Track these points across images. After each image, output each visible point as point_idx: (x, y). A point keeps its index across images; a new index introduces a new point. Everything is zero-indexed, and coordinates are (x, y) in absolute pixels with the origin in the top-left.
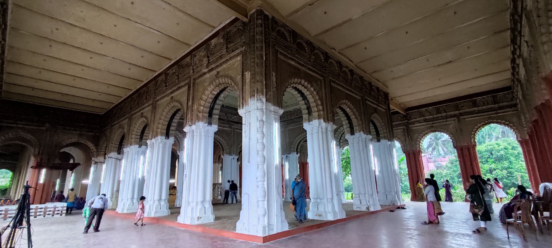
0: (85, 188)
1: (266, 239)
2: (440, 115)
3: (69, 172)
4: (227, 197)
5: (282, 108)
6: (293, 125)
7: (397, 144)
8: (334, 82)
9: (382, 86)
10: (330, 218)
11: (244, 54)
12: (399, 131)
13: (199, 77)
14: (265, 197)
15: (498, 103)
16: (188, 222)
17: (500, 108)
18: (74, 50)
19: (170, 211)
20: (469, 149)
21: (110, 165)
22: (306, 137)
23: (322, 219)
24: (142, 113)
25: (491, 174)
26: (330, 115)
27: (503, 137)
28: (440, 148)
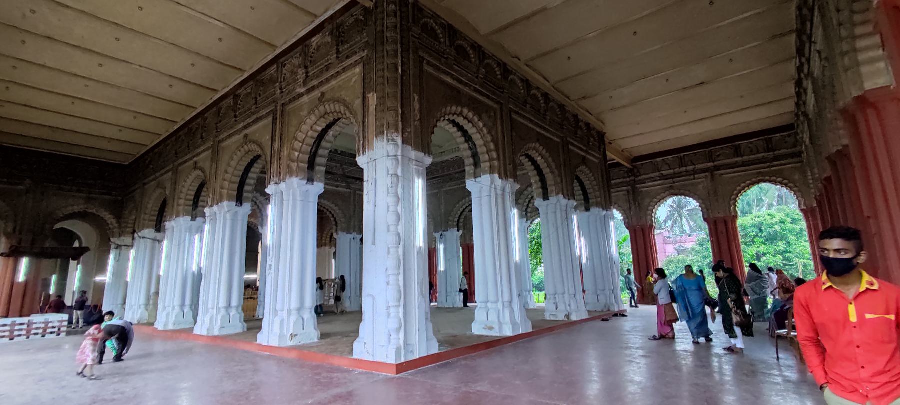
1: (401, 368)
2: (684, 169)
3: (73, 263)
4: (337, 305)
6: (450, 184)
7: (618, 215)
8: (518, 113)
9: (595, 120)
10: (508, 332)
11: (366, 63)
12: (619, 194)
14: (400, 301)
15: (774, 151)
16: (275, 343)
17: (776, 159)
18: (69, 50)
19: (246, 325)
20: (726, 223)
22: (471, 205)
23: (494, 335)
24: (196, 163)
28: (684, 221)
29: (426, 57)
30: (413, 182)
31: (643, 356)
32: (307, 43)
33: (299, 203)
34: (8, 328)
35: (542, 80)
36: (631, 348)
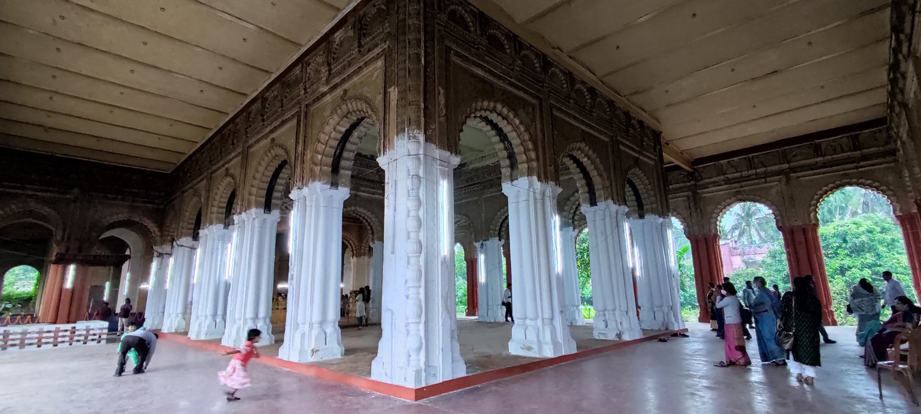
0: (144, 296)
1: (420, 393)
2: (754, 171)
4: (359, 317)
5: (456, 154)
7: (676, 222)
8: (560, 110)
9: (649, 118)
10: (549, 353)
11: (387, 55)
12: (679, 200)
13: (314, 101)
15: (860, 149)
16: (295, 359)
17: (865, 158)
19: (273, 337)
20: (804, 231)
21: (180, 260)
24: (227, 169)
25: (844, 275)
26: (551, 169)
27: (864, 212)
28: (753, 231)
29: (454, 47)
30: (437, 183)
31: (708, 388)
32: (331, 38)
33: (322, 209)
34: (52, 335)
35: (588, 73)
36: (692, 376)
